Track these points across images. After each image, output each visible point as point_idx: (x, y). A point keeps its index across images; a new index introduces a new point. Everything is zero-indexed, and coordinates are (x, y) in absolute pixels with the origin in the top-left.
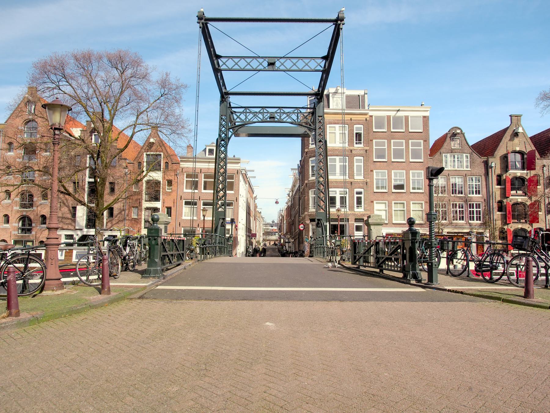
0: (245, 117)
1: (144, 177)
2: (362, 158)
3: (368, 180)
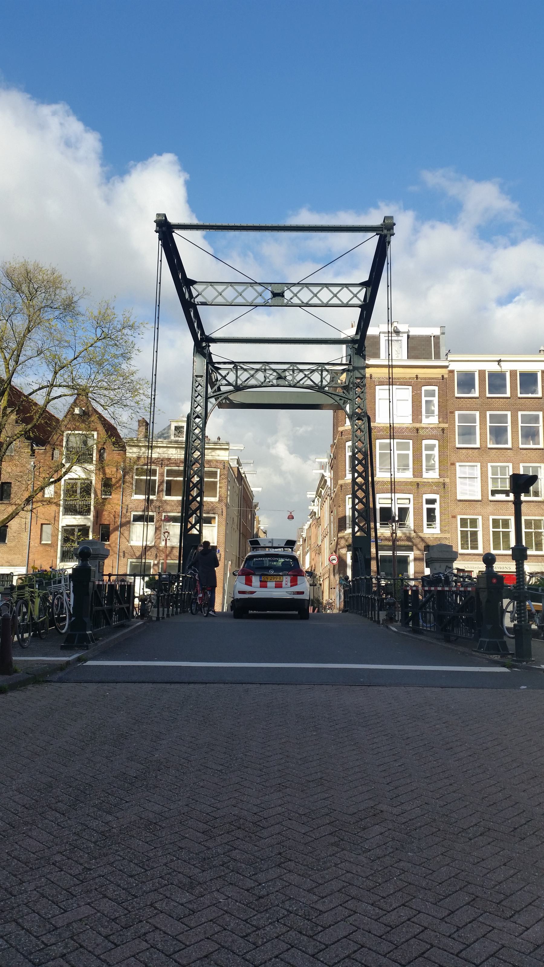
0: (234, 378)
1: (66, 473)
2: (436, 442)
3: (447, 480)
